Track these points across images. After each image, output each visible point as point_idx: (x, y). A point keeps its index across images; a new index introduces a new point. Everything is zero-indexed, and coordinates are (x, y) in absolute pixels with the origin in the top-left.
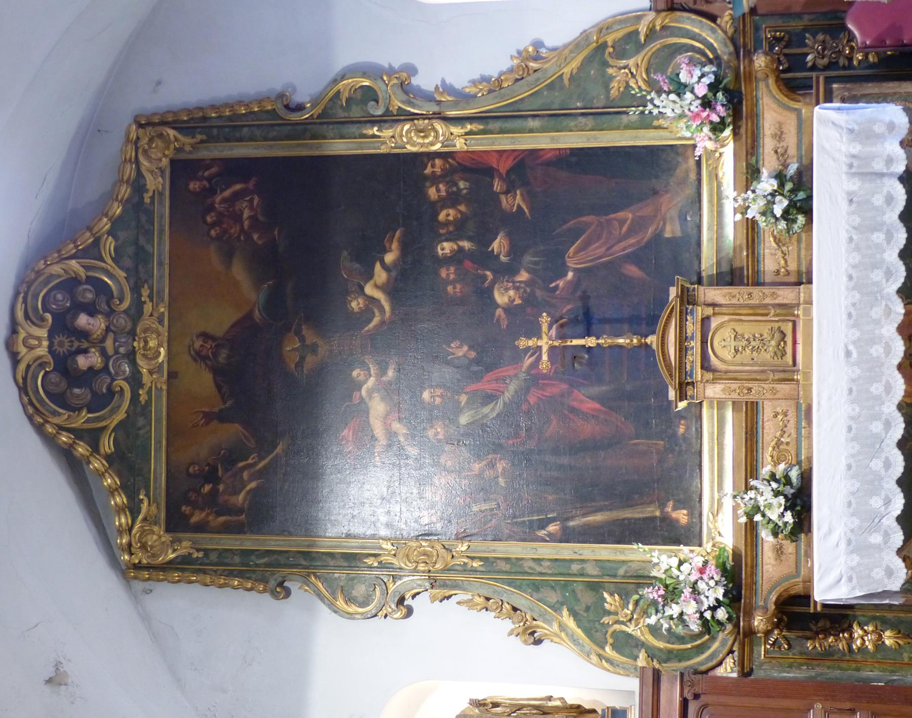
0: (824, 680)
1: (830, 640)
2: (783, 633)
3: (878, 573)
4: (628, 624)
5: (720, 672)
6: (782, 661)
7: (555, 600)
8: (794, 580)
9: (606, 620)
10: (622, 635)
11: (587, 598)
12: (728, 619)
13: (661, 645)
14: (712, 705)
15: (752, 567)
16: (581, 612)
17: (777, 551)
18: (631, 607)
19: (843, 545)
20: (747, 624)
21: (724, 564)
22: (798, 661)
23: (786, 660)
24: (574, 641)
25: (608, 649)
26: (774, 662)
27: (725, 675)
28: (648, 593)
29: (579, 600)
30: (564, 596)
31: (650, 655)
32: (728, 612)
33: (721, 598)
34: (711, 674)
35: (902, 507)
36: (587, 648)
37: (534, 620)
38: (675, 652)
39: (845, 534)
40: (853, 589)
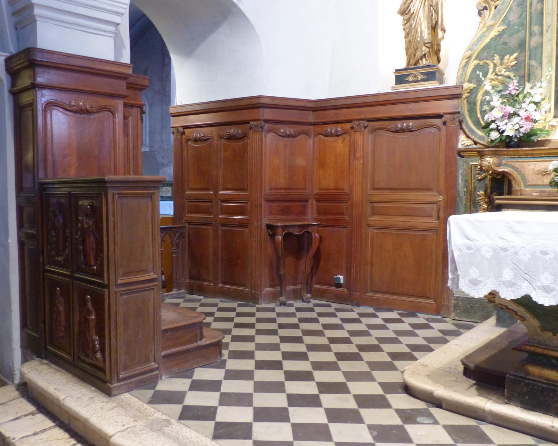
0: (457, 202)
1: (484, 205)
2: (489, 176)
3: (474, 273)
4: (494, 73)
5: (462, 137)
6: (469, 175)
7: (511, 19)
8: (522, 184)
9: (497, 57)
10: (486, 70)
11: (513, 42)
12: (491, 140)
13: (479, 97)
14: (440, 133)
15: (532, 154)
16: (502, 40)
17: (545, 172)
18: (507, 74)
19: (501, 244)
20: (487, 153)
21: (532, 135)
22: (470, 186)
23: (470, 178)
24: (480, 38)
25: (476, 62)
26: (469, 170)
27: (460, 140)
28: (514, 82)
29: (511, 36)
30: (514, 25)
31: (472, 91)
32: (496, 139)
33: (505, 134)
34: (461, 131)
35: (540, 302)
36: (475, 48)
37: (496, 7)
38: (474, 107)
39: (513, 247)
40: (460, 250)
